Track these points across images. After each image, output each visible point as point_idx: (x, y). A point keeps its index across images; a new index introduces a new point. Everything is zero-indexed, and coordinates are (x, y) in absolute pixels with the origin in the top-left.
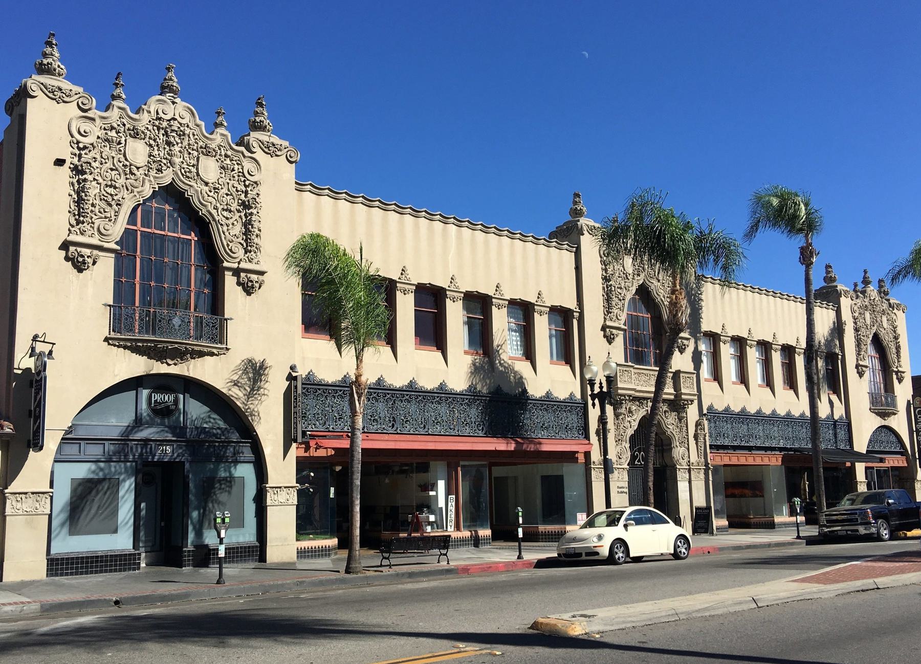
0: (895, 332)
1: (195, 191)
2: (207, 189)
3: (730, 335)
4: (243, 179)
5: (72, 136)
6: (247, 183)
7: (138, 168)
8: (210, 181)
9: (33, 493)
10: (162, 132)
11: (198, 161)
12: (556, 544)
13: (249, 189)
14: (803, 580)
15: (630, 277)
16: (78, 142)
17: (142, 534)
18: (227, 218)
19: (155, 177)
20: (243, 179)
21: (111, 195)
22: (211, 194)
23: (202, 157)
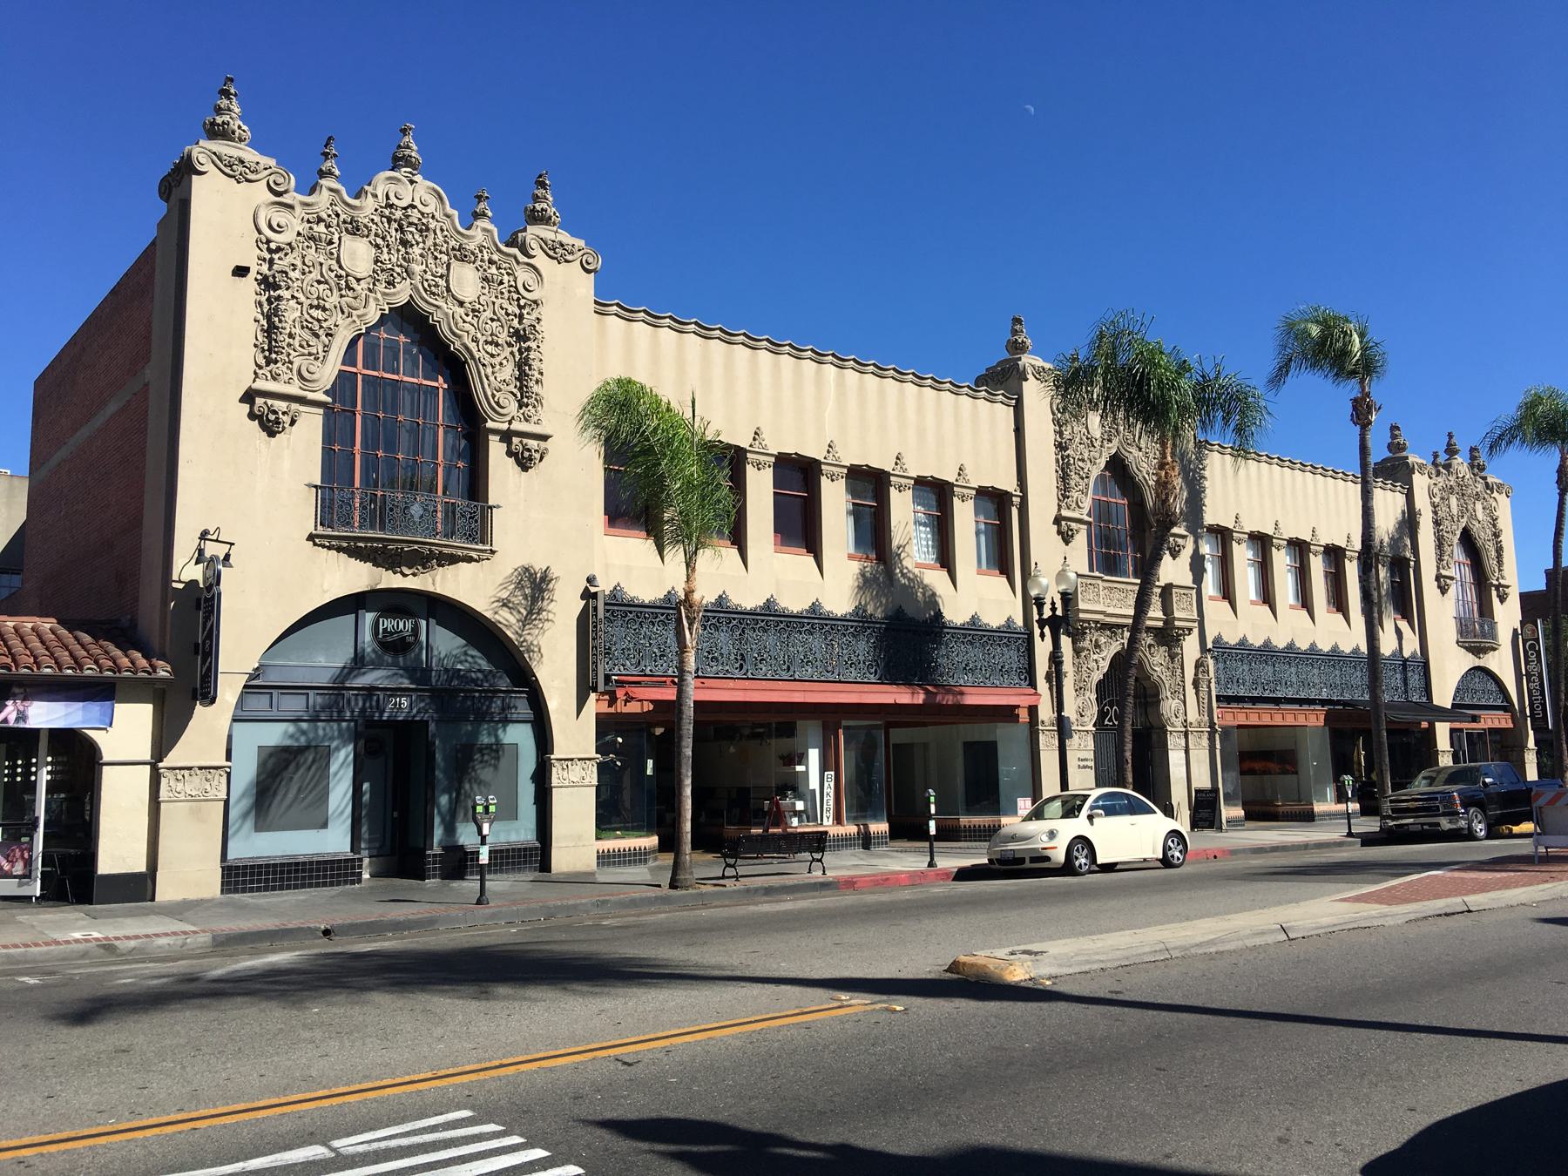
1: (444, 314)
2: (462, 311)
3: (1247, 530)
5: (260, 232)
6: (522, 302)
7: (358, 280)
16: (268, 241)
18: (492, 356)
19: (384, 294)
22: (468, 319)
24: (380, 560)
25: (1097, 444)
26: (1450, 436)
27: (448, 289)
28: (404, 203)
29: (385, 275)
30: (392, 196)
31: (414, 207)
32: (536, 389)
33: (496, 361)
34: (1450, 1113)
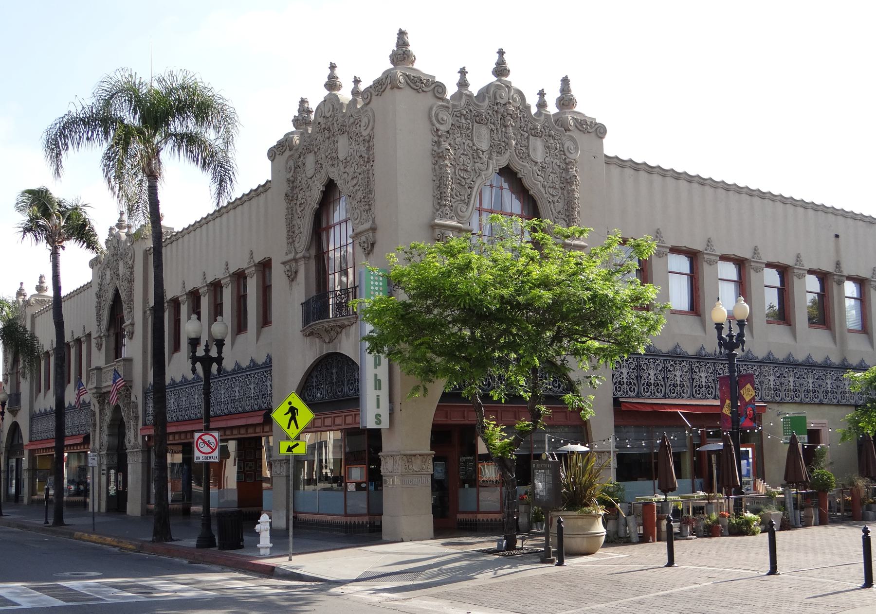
0: (566, 170)
1: (525, 170)
2: (535, 168)
3: (719, 253)
4: (564, 157)
5: (433, 125)
6: (567, 161)
7: (483, 152)
8: (539, 161)
9: (420, 455)
10: (500, 116)
11: (528, 142)
12: (103, 508)
13: (442, 140)
14: (37, 589)
15: (485, 157)
16: (437, 130)
17: (153, 486)
18: (553, 196)
19: (497, 160)
20: (564, 157)
21: (464, 178)
22: (539, 173)
23: (531, 137)
24: (238, 201)
25: (485, 157)
26: (333, 67)
27: (529, 156)
28: (503, 102)
29: (497, 148)
30: (498, 97)
31: (510, 103)
32: (435, 178)
33: (556, 199)
34: (862, 553)
